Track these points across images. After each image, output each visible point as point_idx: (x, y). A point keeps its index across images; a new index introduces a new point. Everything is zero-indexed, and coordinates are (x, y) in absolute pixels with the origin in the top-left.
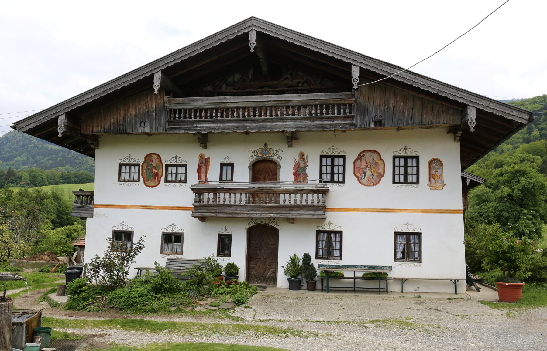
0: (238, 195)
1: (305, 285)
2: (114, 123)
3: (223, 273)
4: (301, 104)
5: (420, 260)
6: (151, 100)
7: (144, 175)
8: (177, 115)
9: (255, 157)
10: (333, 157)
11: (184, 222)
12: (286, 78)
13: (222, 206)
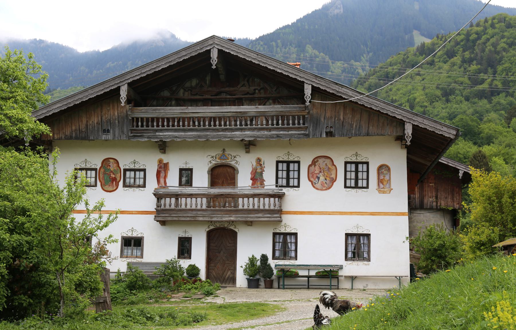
0: (199, 200)
1: (262, 283)
2: (76, 130)
3: (185, 274)
4: (258, 115)
5: (369, 260)
6: (113, 108)
7: (101, 179)
8: (140, 124)
9: (214, 162)
10: (288, 163)
11: (146, 227)
12: (244, 85)
13: (183, 210)
